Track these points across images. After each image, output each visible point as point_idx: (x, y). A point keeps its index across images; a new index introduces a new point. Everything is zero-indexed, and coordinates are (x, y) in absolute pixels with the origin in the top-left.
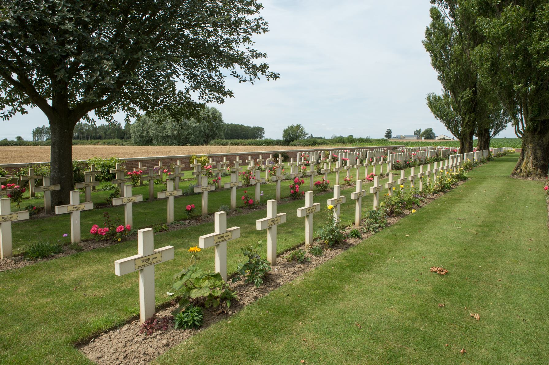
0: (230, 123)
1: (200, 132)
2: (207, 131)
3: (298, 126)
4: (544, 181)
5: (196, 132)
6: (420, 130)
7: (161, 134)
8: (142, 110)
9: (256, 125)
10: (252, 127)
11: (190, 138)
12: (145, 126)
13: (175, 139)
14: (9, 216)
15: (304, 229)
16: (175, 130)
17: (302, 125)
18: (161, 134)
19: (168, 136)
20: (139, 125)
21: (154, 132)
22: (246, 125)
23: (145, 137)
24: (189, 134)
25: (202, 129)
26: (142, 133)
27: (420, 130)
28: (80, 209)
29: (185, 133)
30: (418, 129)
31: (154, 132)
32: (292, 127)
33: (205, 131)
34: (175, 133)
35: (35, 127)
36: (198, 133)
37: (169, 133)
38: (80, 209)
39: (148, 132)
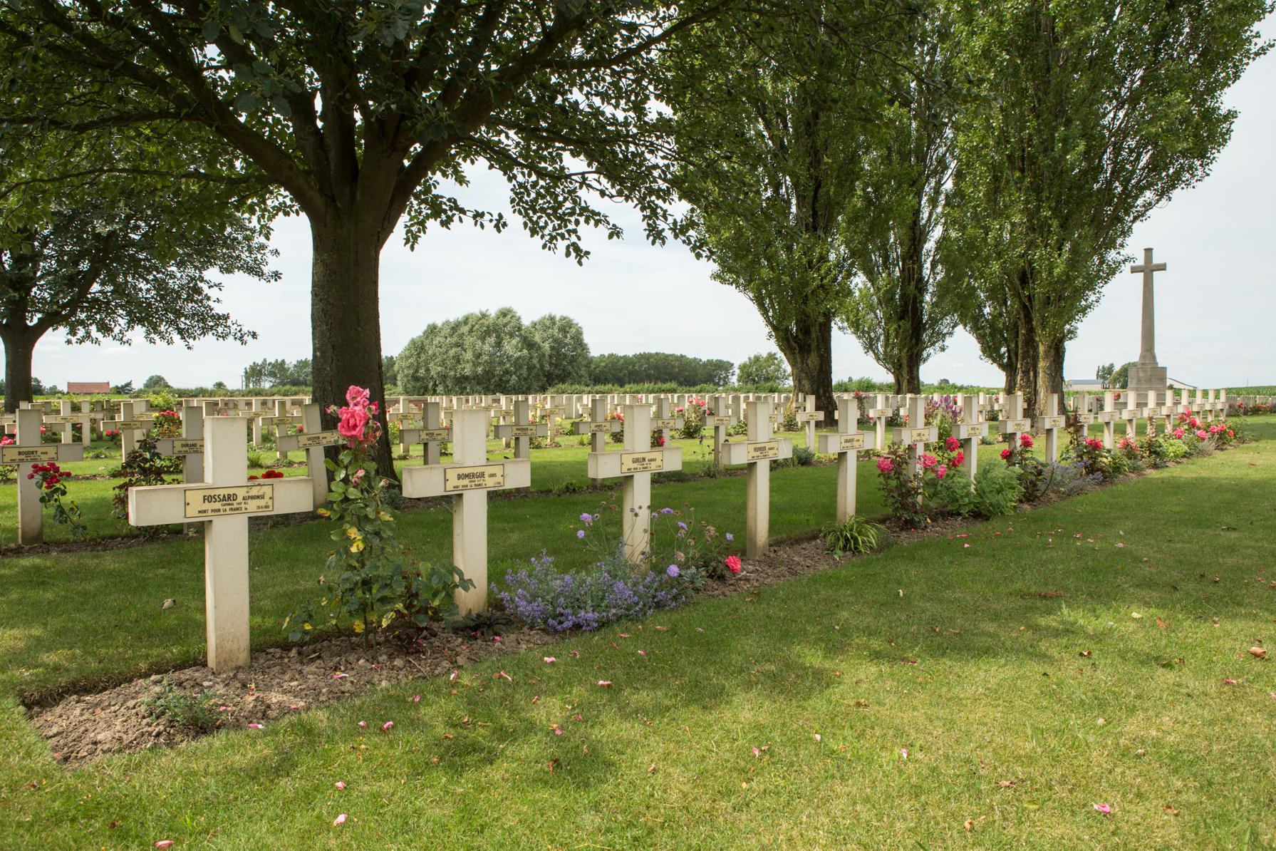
0: (653, 352)
1: (531, 368)
2: (547, 367)
3: (504, 313)
4: (1236, 637)
5: (521, 367)
6: (1112, 365)
7: (452, 373)
8: (228, 291)
9: (715, 357)
10: (704, 359)
11: (508, 381)
12: (423, 357)
13: (479, 383)
14: (241, 493)
15: (774, 508)
16: (479, 364)
17: (578, 319)
18: (452, 373)
19: (466, 378)
20: (412, 356)
21: (439, 369)
22: (690, 356)
23: (423, 379)
24: (507, 372)
25: (535, 361)
26: (417, 371)
27: (1112, 365)
28: (653, 465)
29: (498, 371)
30: (1107, 365)
31: (439, 369)
32: (757, 359)
33: (542, 366)
34: (480, 370)
35: (248, 364)
36: (524, 371)
37: (468, 370)
38: (653, 465)
39: (428, 370)
